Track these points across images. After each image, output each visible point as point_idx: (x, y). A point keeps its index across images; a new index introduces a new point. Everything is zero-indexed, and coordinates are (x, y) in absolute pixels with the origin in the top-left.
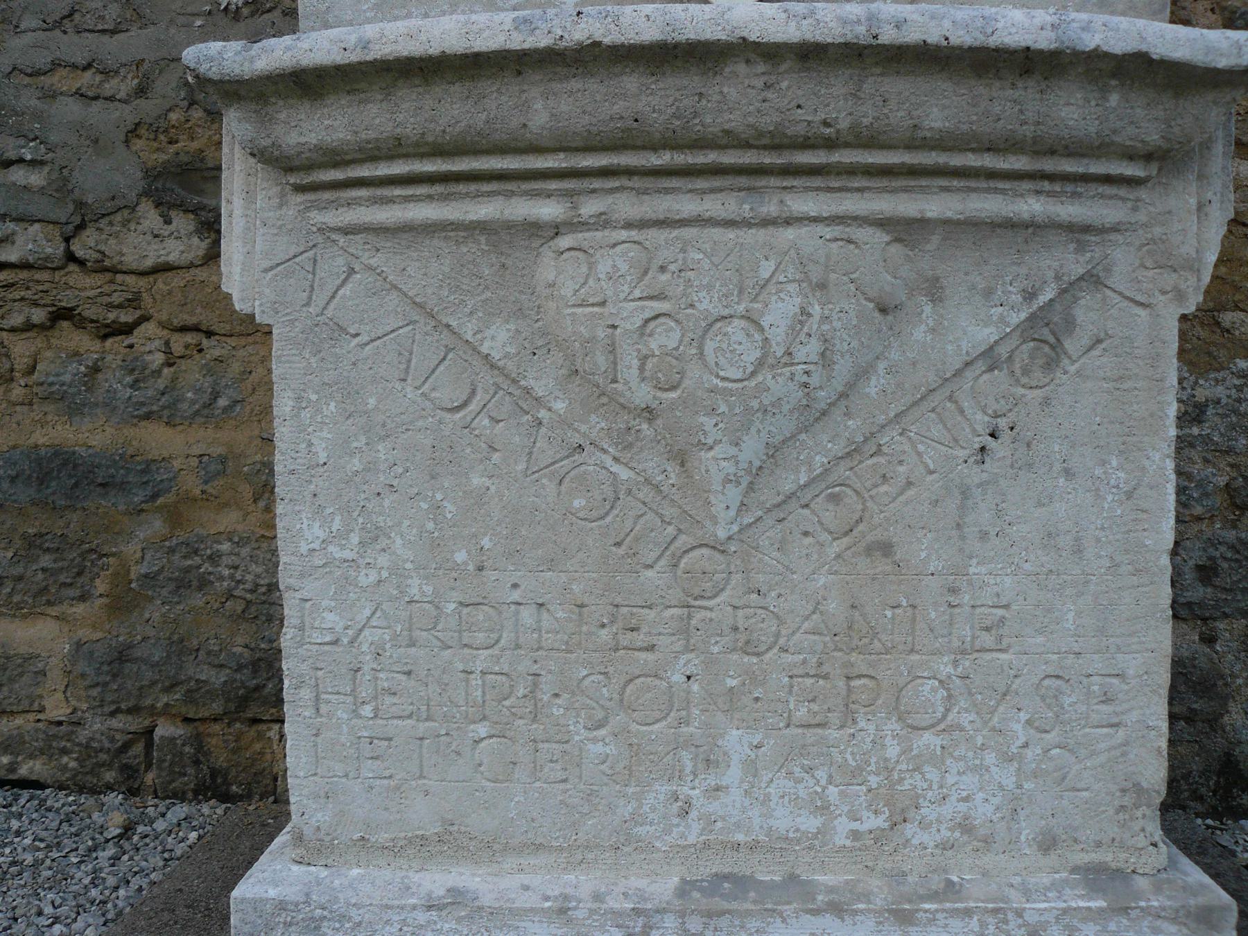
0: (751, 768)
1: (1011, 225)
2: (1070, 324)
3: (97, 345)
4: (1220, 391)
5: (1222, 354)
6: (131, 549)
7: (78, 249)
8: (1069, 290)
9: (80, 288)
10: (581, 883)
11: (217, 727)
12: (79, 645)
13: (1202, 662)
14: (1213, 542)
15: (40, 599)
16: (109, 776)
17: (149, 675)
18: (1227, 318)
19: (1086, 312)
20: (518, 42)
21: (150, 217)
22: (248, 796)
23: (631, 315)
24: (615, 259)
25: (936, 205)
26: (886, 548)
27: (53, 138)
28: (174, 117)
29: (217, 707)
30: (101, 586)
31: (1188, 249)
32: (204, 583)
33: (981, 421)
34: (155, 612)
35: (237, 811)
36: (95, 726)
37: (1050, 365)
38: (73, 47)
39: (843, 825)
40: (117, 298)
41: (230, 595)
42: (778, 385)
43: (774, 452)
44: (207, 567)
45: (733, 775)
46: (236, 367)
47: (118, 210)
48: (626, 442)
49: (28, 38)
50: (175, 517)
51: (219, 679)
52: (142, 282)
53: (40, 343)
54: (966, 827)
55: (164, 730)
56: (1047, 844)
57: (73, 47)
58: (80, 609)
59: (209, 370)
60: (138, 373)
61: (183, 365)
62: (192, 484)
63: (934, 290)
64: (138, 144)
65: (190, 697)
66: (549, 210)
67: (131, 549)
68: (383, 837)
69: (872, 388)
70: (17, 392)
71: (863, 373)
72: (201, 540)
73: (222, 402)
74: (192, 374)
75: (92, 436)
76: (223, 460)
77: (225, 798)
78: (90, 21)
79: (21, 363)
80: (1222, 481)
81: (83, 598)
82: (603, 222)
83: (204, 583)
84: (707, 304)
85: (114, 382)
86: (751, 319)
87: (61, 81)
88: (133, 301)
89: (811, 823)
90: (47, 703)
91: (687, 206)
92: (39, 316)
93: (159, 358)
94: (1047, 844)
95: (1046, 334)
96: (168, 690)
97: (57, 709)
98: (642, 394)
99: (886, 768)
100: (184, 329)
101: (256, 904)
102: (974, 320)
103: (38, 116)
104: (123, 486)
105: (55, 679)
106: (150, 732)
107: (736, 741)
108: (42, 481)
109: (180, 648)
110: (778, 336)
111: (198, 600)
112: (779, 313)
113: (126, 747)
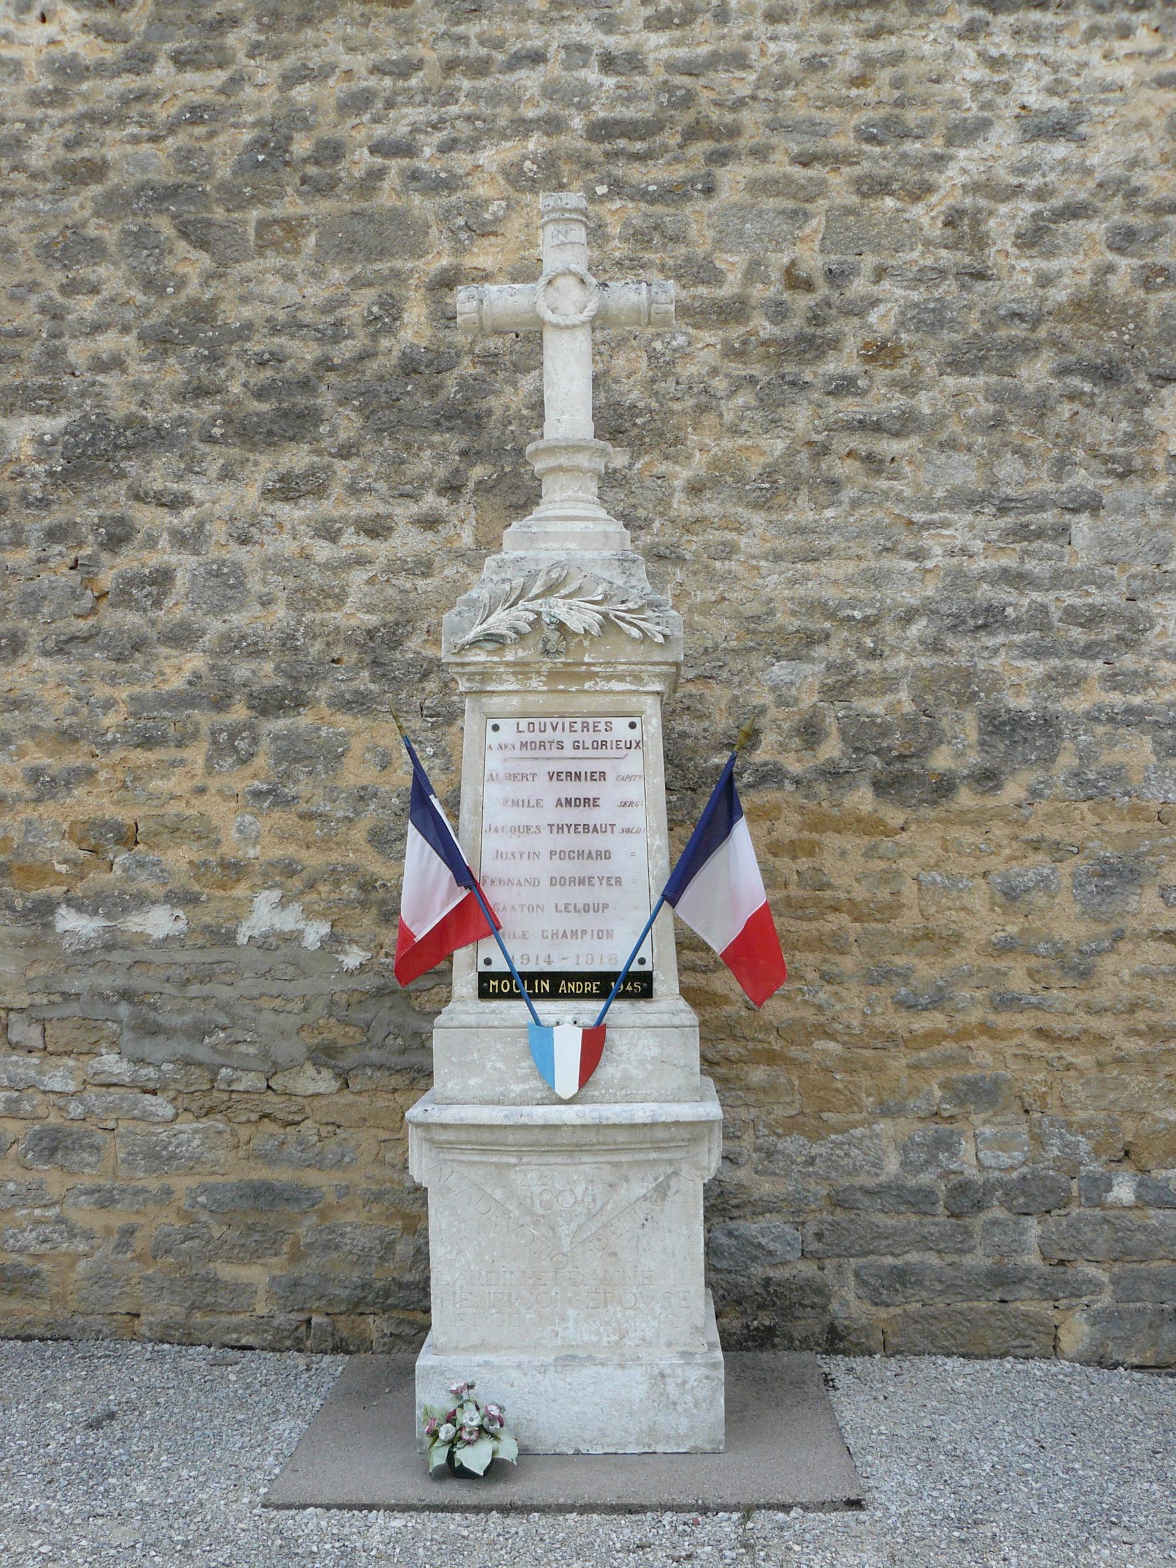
0: (576, 1321)
1: (647, 1161)
2: (669, 1187)
3: (282, 1131)
4: (823, 1150)
5: (824, 1132)
6: (301, 1231)
7: (272, 1084)
8: (668, 1177)
9: (274, 1103)
10: (524, 1358)
11: (343, 1317)
12: (273, 1278)
13: (818, 1280)
14: (821, 1222)
15: (255, 1255)
16: (288, 1343)
17: (309, 1292)
18: (825, 1115)
19: (673, 1183)
20: (505, 1122)
21: (310, 1070)
22: (358, 1351)
23: (537, 1190)
24: (533, 1175)
25: (624, 1158)
26: (615, 1254)
27: (261, 1031)
28: (321, 1022)
29: (343, 1308)
30: (285, 1249)
31: (705, 1163)
32: (337, 1247)
33: (643, 1216)
34: (313, 1261)
35: (355, 1359)
36: (281, 1319)
37: (663, 1199)
38: (274, 988)
39: (605, 1339)
40: (293, 1109)
41: (351, 1253)
42: (579, 1209)
43: (580, 1227)
44: (339, 1239)
45: (571, 1324)
46: (353, 1143)
47: (293, 1066)
48: (537, 1223)
49: (248, 981)
50: (323, 1215)
51: (344, 1293)
52: (306, 1101)
53: (253, 1129)
54: (643, 1339)
55: (316, 1320)
56: (669, 1345)
57: (274, 988)
58: (274, 1260)
59: (340, 1144)
60: (302, 1142)
61: (327, 1141)
62: (332, 1199)
63: (627, 1179)
64: (303, 1034)
65: (330, 1303)
66: (513, 1160)
67: (301, 1231)
68: (462, 1346)
69: (609, 1207)
70: (242, 1153)
71: (605, 1204)
72: (336, 1225)
73: (347, 1159)
74: (332, 1146)
75: (281, 1175)
76: (347, 1187)
77: (347, 1352)
78: (279, 975)
79: (243, 1139)
80: (825, 1193)
81: (276, 1255)
82: (529, 1164)
83: (337, 1247)
84: (558, 1187)
85: (292, 1149)
86: (572, 1191)
87: (264, 1003)
88: (302, 1110)
89: (595, 1339)
90: (257, 1307)
91: (552, 1160)
92: (254, 1117)
93: (316, 1138)
94: (669, 1345)
95: (662, 1190)
96: (319, 1299)
97: (262, 1309)
98: (541, 1211)
99: (617, 1321)
100: (327, 1124)
101: (424, 1367)
102: (639, 1187)
103: (254, 1020)
104: (297, 1200)
105: (262, 1294)
106: (309, 1321)
107: (571, 1313)
108: (256, 1198)
109: (325, 1279)
110: (579, 1194)
111: (334, 1255)
112: (579, 1189)
113: (297, 1328)
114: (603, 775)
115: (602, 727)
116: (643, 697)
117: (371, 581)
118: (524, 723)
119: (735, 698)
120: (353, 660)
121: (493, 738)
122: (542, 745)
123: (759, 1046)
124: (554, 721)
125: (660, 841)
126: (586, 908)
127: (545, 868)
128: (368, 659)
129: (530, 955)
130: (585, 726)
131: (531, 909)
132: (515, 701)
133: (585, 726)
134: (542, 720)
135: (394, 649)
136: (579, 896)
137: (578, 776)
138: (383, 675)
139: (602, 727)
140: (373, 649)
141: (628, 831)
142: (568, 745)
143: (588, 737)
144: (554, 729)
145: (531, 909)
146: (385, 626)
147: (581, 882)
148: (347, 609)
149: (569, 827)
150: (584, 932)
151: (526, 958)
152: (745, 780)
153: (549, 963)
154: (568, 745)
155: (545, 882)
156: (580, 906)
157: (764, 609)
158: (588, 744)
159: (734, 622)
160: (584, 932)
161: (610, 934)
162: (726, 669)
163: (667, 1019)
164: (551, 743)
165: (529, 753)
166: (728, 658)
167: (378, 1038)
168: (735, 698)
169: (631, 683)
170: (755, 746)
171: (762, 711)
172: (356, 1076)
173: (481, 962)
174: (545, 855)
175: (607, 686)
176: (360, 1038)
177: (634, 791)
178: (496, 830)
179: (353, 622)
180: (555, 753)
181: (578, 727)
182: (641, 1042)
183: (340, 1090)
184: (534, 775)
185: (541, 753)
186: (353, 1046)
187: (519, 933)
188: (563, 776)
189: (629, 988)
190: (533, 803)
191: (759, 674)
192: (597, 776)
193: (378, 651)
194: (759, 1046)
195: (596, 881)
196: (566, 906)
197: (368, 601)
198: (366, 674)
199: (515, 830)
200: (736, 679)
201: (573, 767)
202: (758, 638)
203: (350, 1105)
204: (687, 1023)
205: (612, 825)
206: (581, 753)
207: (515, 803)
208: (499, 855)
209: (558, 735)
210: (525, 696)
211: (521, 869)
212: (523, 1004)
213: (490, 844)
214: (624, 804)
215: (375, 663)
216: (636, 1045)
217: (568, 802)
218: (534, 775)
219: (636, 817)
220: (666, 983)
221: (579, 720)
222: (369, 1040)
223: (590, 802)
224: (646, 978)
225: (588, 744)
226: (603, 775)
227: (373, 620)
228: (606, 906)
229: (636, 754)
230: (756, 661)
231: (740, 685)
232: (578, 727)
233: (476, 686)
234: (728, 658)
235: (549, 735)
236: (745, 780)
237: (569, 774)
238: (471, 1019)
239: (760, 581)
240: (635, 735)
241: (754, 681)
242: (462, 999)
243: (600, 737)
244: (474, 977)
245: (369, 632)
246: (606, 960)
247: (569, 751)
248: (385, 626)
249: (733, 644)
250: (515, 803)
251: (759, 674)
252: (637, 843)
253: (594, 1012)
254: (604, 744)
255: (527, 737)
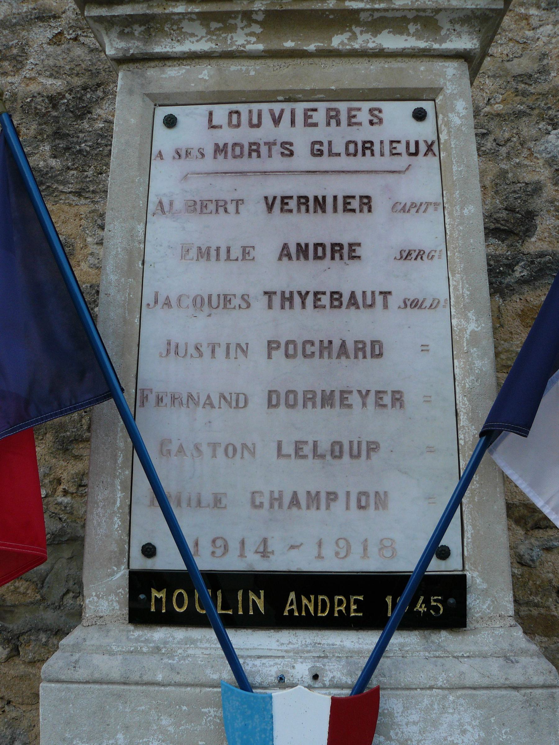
46: (25, 723)
59: (9, 725)
114: (366, 202)
115: (363, 117)
116: (439, 64)
117: (57, 40)
118: (221, 112)
119: (503, 174)
120: (32, 132)
121: (164, 139)
122: (254, 149)
123: (535, 612)
124: (277, 107)
125: (476, 325)
126: (337, 450)
127: (259, 373)
128: (49, 130)
129: (229, 542)
130: (333, 117)
131: (231, 451)
132: (205, 75)
133: (333, 117)
134: (255, 107)
135: (81, 117)
136: (322, 425)
137: (320, 204)
138: (67, 149)
139: (363, 117)
140: (56, 119)
141: (416, 304)
142: (302, 148)
143: (338, 136)
144: (277, 121)
145: (231, 451)
146: (70, 91)
147: (327, 400)
148: (26, 72)
149: (303, 297)
150: (332, 496)
151: (220, 545)
152: (517, 275)
153: (265, 554)
154: (302, 148)
155: (258, 401)
156: (324, 446)
157: (536, 67)
158: (338, 147)
159: (499, 81)
160: (332, 496)
161: (382, 500)
162: (491, 138)
163: (495, 670)
164: (270, 145)
165: (231, 164)
166: (492, 125)
167: (55, 597)
168: (503, 174)
169: (418, 35)
170: (529, 231)
171: (537, 189)
172: (29, 642)
173: (136, 551)
174: (258, 349)
175: (373, 42)
176: (33, 596)
177: (424, 232)
178: (168, 303)
179: (34, 88)
180: (277, 162)
181: (320, 117)
182: (447, 719)
183: (8, 658)
184: (238, 202)
185: (254, 164)
186: (27, 605)
187: (207, 498)
188: (293, 204)
189: (421, 608)
190: (236, 252)
191: (531, 144)
192: (355, 204)
193: (62, 121)
194: (535, 612)
195: (355, 399)
196: (298, 446)
197: (51, 62)
198: (46, 148)
199: (204, 303)
200: (503, 150)
201: (311, 188)
202: (530, 101)
203: (21, 678)
204: (537, 680)
205: (385, 294)
206: (325, 163)
207: (204, 254)
208: (172, 349)
209: (284, 132)
210: (224, 63)
211: (209, 376)
212: (210, 634)
213: (156, 328)
214: (406, 255)
215: (58, 134)
216: (435, 724)
217: (302, 251)
218: (238, 202)
219: (431, 279)
220: (491, 596)
221: (322, 106)
222: (43, 599)
223: (344, 252)
224: (456, 585)
225: (338, 147)
226: (366, 202)
227: (55, 85)
228: (373, 447)
229: (426, 165)
230: (527, 129)
231: (508, 157)
232: (320, 117)
233: (135, 46)
234: (492, 125)
235: (267, 132)
236: (517, 275)
237: (303, 200)
238: (109, 666)
239: (530, 34)
240: (424, 131)
241: (526, 152)
242: (100, 622)
243: (361, 135)
244: (121, 576)
245: (51, 99)
246: (373, 550)
247: (303, 159)
248: (70, 91)
249: (499, 107)
250: (204, 254)
251: (531, 144)
252: (433, 327)
253: (350, 654)
254: (367, 147)
255: (227, 136)
